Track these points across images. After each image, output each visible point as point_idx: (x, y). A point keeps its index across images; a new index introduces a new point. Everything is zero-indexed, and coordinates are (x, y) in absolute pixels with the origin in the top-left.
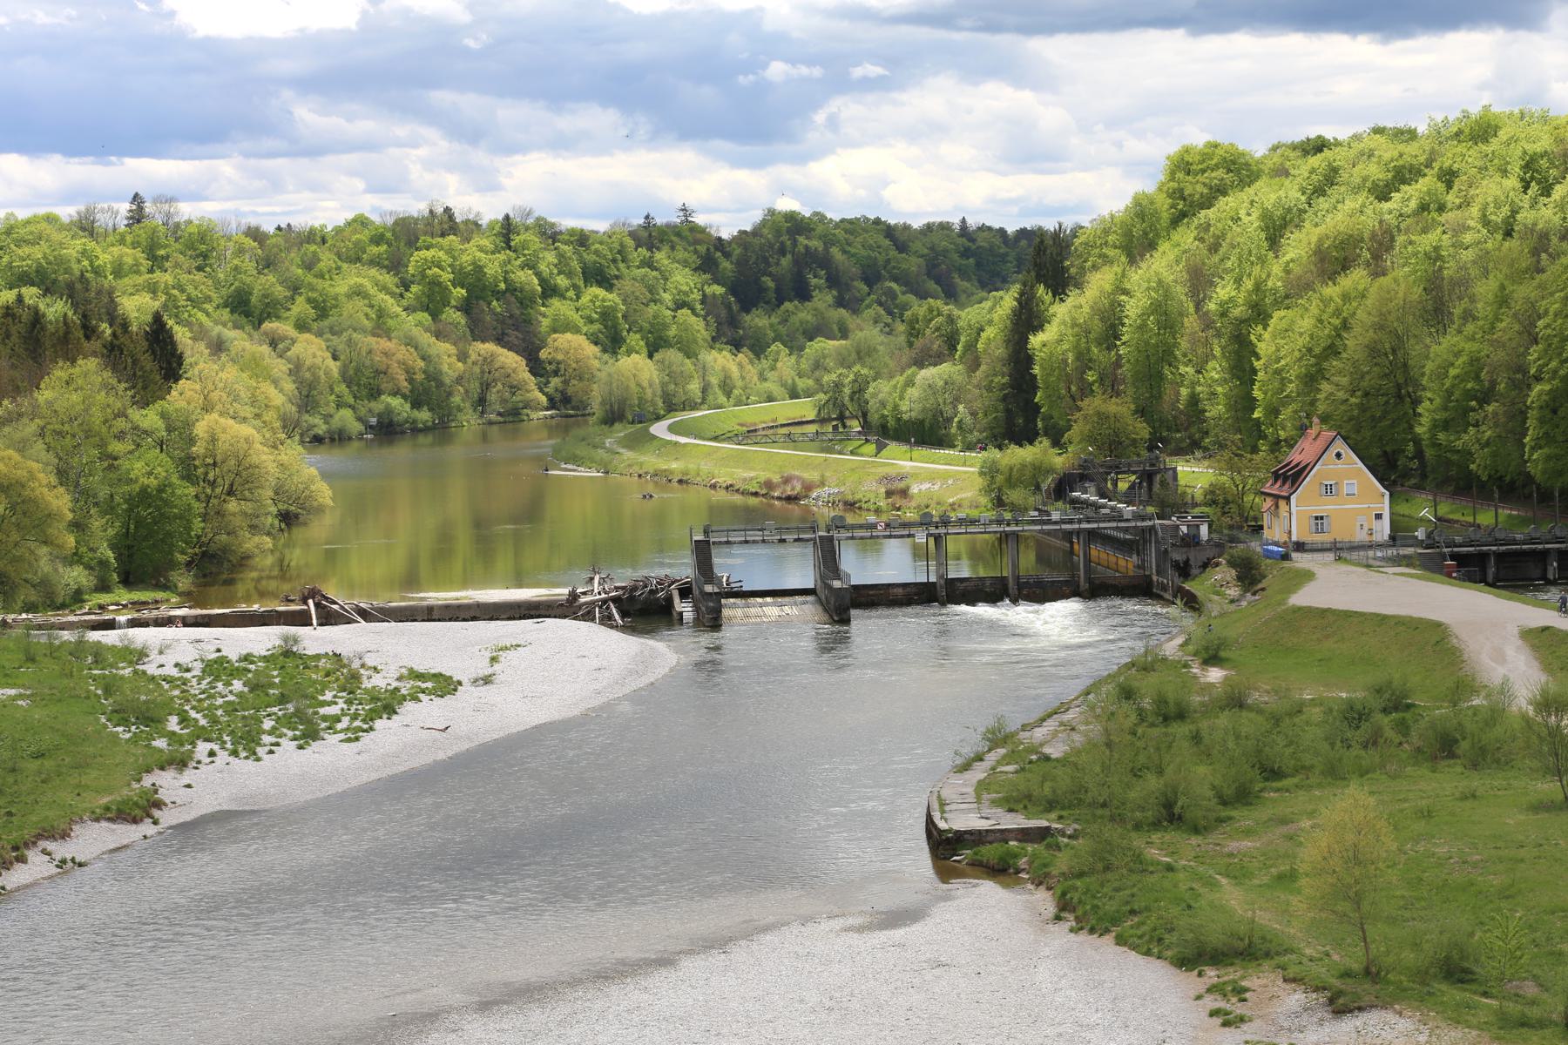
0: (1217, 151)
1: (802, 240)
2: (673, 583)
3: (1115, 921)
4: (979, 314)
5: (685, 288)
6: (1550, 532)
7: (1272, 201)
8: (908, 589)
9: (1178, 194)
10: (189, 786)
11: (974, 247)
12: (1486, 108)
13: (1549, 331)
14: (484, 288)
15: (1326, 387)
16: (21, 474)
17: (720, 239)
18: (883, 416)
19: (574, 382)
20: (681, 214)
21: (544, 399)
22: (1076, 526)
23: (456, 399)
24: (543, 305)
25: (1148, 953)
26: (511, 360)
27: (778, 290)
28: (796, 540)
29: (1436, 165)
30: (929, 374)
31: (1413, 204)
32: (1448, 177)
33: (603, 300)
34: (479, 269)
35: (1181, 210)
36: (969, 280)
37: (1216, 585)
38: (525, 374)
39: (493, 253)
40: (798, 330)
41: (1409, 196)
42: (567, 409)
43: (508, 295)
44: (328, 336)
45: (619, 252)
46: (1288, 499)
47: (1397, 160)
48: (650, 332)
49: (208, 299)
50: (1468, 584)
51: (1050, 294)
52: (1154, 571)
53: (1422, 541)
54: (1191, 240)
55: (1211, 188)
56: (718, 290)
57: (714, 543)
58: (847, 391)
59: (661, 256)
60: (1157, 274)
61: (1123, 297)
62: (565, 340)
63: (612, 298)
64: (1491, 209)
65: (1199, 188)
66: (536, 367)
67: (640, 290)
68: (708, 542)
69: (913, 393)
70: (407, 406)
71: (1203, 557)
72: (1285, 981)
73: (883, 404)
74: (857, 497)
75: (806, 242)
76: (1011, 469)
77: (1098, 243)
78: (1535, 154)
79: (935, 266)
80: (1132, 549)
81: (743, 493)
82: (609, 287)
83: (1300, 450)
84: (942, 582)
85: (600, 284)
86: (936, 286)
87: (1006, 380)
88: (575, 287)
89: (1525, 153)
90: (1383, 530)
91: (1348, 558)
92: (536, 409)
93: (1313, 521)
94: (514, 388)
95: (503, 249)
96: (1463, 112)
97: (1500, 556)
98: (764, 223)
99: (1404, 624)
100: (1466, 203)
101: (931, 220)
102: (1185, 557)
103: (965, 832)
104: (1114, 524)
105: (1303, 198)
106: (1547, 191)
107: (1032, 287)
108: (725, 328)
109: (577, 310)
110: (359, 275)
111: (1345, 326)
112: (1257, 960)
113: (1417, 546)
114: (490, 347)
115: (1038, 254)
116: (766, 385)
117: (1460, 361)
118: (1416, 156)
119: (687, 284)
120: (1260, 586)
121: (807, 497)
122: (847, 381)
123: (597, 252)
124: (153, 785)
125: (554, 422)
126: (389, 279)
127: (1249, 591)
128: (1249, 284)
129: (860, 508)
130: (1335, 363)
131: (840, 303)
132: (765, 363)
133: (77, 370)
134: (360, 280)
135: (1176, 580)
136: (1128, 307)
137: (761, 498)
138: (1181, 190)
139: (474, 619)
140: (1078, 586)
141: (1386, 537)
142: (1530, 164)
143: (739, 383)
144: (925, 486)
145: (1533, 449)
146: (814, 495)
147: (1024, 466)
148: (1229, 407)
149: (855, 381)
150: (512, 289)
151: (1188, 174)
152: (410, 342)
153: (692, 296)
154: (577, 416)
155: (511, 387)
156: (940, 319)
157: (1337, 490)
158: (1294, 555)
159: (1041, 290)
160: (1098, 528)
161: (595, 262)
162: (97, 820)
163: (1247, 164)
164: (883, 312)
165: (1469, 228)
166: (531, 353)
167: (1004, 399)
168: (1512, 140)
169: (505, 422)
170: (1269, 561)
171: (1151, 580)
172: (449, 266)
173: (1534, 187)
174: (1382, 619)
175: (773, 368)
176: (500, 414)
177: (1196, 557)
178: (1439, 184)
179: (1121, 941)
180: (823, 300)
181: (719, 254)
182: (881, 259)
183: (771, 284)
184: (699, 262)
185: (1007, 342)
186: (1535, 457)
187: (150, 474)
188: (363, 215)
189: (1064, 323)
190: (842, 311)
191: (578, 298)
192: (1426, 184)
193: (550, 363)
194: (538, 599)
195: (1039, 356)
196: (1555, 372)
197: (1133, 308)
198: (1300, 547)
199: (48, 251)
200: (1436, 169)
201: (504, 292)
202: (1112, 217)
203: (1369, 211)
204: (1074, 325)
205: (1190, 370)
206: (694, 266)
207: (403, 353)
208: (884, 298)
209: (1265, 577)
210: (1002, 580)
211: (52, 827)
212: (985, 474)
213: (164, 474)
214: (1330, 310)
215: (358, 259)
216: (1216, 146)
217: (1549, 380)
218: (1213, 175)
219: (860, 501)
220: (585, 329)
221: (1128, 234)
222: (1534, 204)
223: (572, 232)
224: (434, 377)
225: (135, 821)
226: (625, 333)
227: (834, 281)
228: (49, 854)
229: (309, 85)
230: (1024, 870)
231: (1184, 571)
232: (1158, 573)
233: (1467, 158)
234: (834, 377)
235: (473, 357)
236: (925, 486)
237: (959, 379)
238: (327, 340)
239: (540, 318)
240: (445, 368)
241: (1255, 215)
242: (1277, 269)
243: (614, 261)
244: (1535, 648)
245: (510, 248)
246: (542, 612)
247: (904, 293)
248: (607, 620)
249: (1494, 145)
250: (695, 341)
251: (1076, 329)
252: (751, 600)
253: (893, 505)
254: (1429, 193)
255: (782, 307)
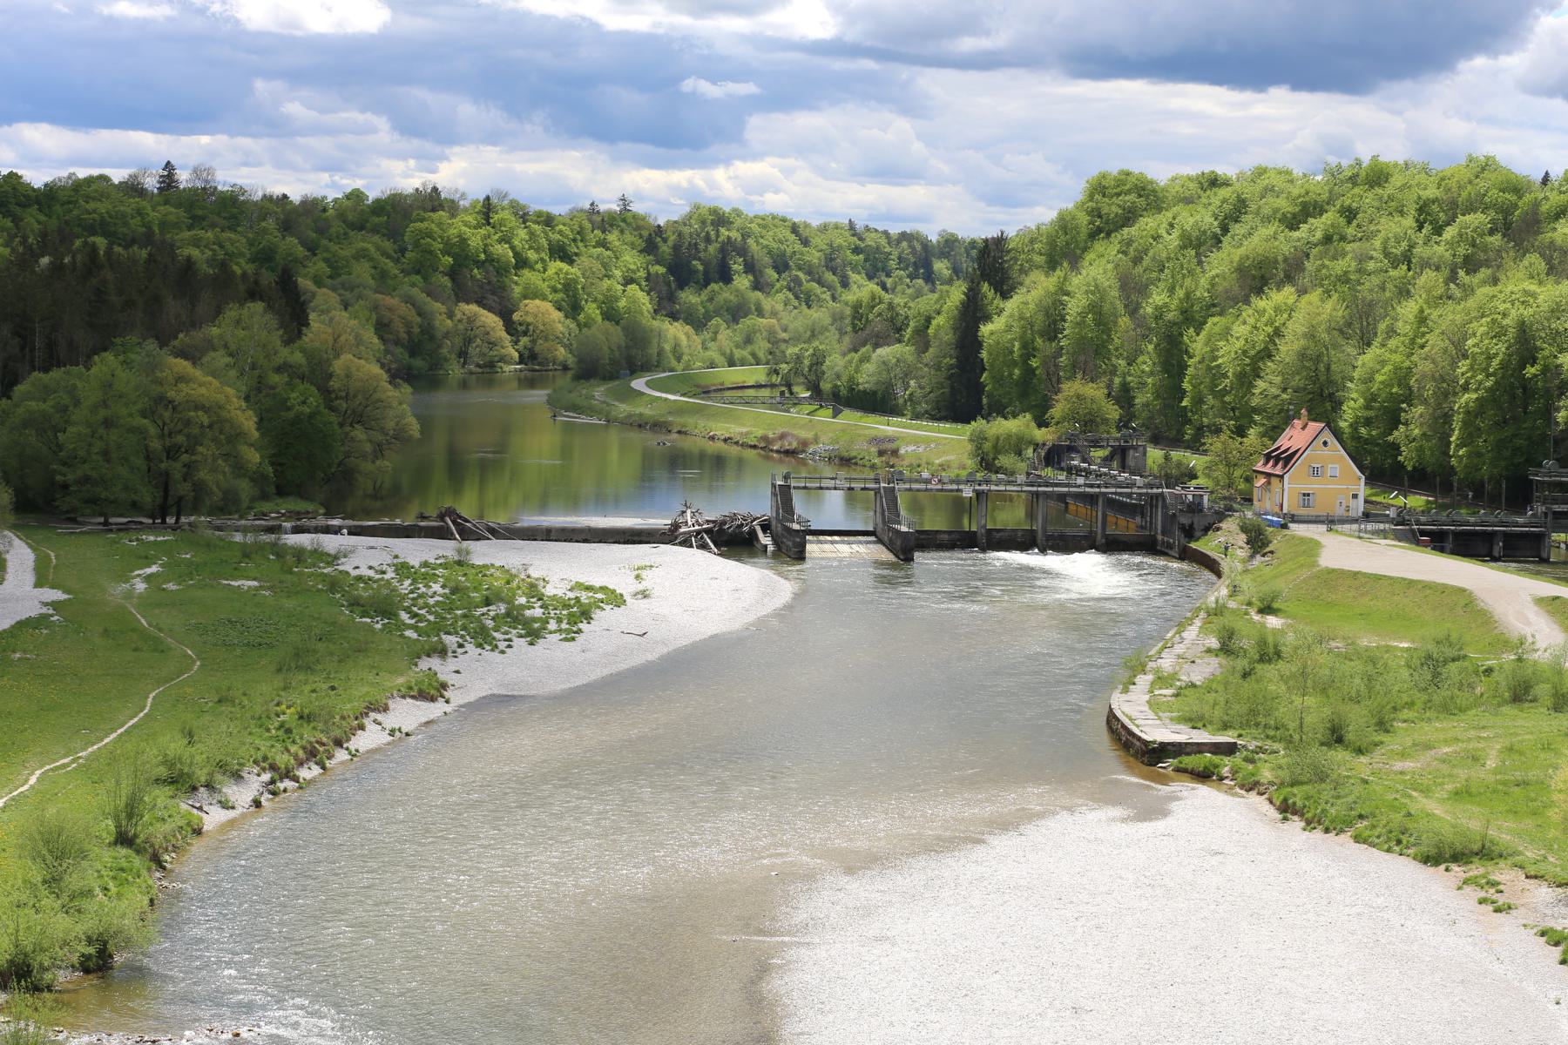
0: (1129, 178)
1: (722, 230)
2: (755, 520)
3: (1350, 824)
4: (928, 304)
5: (632, 267)
6: (1448, 516)
7: (1191, 223)
8: (953, 536)
9: (1096, 213)
10: (458, 672)
11: (863, 245)
12: (1375, 158)
13: (1476, 350)
14: (466, 257)
15: (1261, 385)
16: (221, 398)
17: (659, 226)
18: (836, 386)
19: (540, 341)
20: (621, 203)
21: (516, 355)
22: (1097, 490)
23: (444, 351)
24: (516, 275)
25: (1389, 850)
26: (490, 320)
27: (706, 273)
28: (862, 489)
29: (1338, 204)
30: (883, 352)
31: (1319, 235)
32: (1350, 214)
33: (567, 273)
34: (463, 241)
35: (1098, 227)
36: (859, 273)
37: (1225, 541)
38: (500, 332)
39: (475, 228)
40: (722, 307)
41: (1317, 227)
42: (533, 364)
43: (487, 264)
44: (341, 291)
45: (579, 233)
46: (1281, 477)
47: (1304, 197)
48: (604, 303)
49: (242, 254)
50: (652, 529)
51: (992, 291)
52: (1159, 531)
53: (1393, 519)
54: (1115, 252)
55: (1124, 210)
56: (661, 270)
57: (794, 488)
58: (807, 362)
59: (613, 237)
60: (1095, 280)
61: (1065, 298)
62: (534, 305)
63: (574, 271)
64: (1392, 243)
65: (1115, 209)
66: (510, 327)
67: (597, 266)
68: (789, 487)
69: (869, 367)
70: (406, 356)
71: (1205, 523)
72: (1527, 877)
73: (838, 377)
74: (853, 454)
75: (727, 233)
76: (998, 438)
77: (1026, 250)
78: (1428, 199)
79: (832, 260)
80: (1135, 512)
81: (742, 445)
82: (571, 262)
83: (1289, 436)
84: (983, 531)
85: (562, 259)
86: (833, 277)
87: (953, 361)
88: (542, 260)
89: (1419, 198)
90: (1359, 507)
91: (1340, 530)
92: (508, 363)
93: (1302, 497)
94: (493, 345)
95: (484, 225)
96: (1356, 159)
97: (1457, 534)
98: (690, 216)
99: (1430, 588)
100: (1368, 237)
101: (828, 220)
102: (1190, 521)
103: (1169, 744)
104: (1113, 490)
105: (1216, 223)
106: (1438, 231)
107: (979, 283)
108: (665, 303)
109: (544, 280)
110: (364, 241)
111: (1278, 333)
112: (1492, 859)
113: (1387, 522)
114: (473, 308)
115: (983, 256)
116: (709, 353)
117: (1386, 369)
118: (1320, 194)
119: (635, 263)
120: (1268, 549)
121: (803, 451)
122: (807, 354)
123: (560, 232)
124: (430, 669)
125: (522, 374)
126: (388, 245)
127: (1258, 553)
128: (1180, 293)
129: (856, 464)
130: (1269, 364)
131: (757, 286)
132: (707, 335)
133: (245, 312)
134: (365, 245)
135: (1182, 540)
136: (1069, 306)
137: (760, 451)
138: (1099, 210)
139: (586, 541)
140: (1095, 541)
141: (1360, 514)
142: (1423, 208)
143: (686, 351)
144: (911, 448)
145: (1459, 447)
146: (811, 450)
147: (1009, 436)
148: (1158, 396)
149: (814, 355)
150: (491, 259)
151: (1104, 196)
152: (409, 300)
153: (639, 274)
154: (541, 371)
155: (490, 343)
156: (882, 306)
157: (1323, 473)
158: (1291, 525)
159: (985, 287)
160: (1006, 491)
161: (559, 241)
162: (403, 697)
163: (1154, 191)
164: (792, 297)
165: (1371, 258)
166: (506, 314)
167: (950, 377)
168: (1405, 187)
169: (483, 373)
170: (1271, 529)
171: (1156, 539)
172: (440, 237)
173: (1427, 228)
174: (1411, 583)
175: (714, 339)
176: (478, 366)
177: (1199, 522)
178: (1341, 219)
179: (1358, 839)
180: (742, 282)
181: (658, 239)
182: (789, 251)
183: (701, 268)
184: (644, 245)
185: (955, 329)
186: (1461, 453)
187: (304, 402)
188: (358, 189)
189: (1011, 316)
190: (758, 294)
191: (545, 270)
192: (1330, 217)
193: (520, 324)
194: (641, 527)
195: (988, 342)
196: (1480, 383)
197: (1074, 306)
198: (1294, 519)
199: (110, 207)
200: (1338, 207)
201: (484, 262)
202: (1038, 228)
203: (1281, 237)
204: (1021, 318)
205: (1122, 362)
206: (639, 248)
207: (405, 310)
208: (792, 285)
209: (1271, 542)
210: (1032, 533)
211: (376, 701)
212: (973, 441)
213: (315, 404)
214: (1264, 319)
215: (361, 228)
216: (1128, 174)
217: (1476, 390)
218: (1127, 198)
219: (855, 458)
220: (550, 297)
221: (1052, 243)
222: (1427, 242)
223: (539, 214)
224: (428, 331)
225: (433, 699)
226: (583, 302)
227: (750, 268)
228: (380, 724)
229: (297, 77)
230: (1227, 777)
231: (1190, 533)
232: (1163, 533)
233: (1368, 199)
234: (796, 350)
235: (459, 316)
236: (911, 448)
237: (910, 359)
238: (340, 295)
239: (513, 286)
240: (437, 323)
241: (1176, 233)
242: (1204, 282)
243: (574, 240)
244: (1551, 613)
245: (489, 224)
246: (643, 539)
247: (808, 281)
248: (703, 546)
249: (1389, 190)
250: (641, 313)
251: (1022, 322)
252: (821, 538)
253: (887, 463)
254: (1332, 225)
255: (709, 288)
